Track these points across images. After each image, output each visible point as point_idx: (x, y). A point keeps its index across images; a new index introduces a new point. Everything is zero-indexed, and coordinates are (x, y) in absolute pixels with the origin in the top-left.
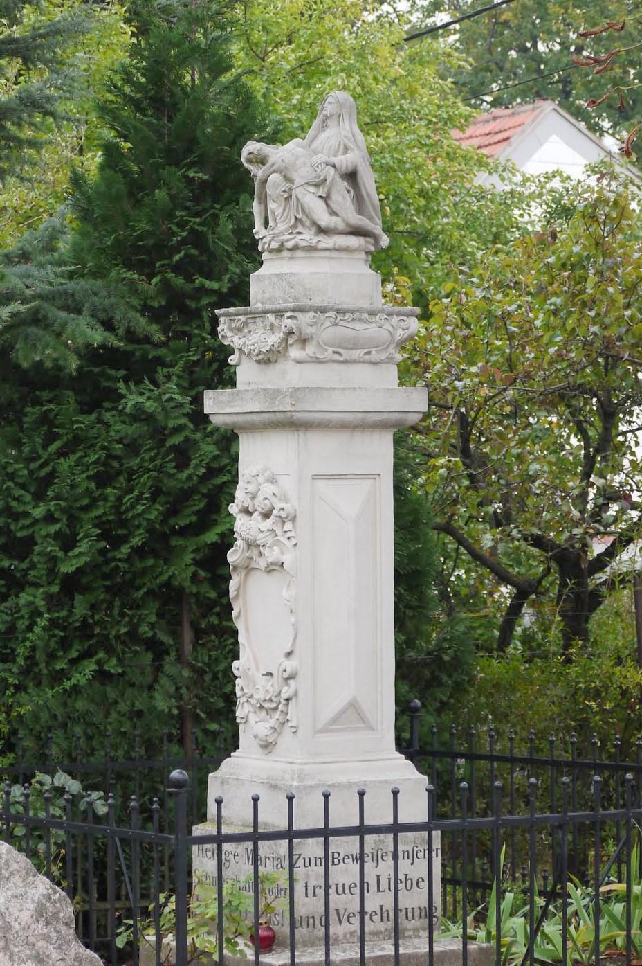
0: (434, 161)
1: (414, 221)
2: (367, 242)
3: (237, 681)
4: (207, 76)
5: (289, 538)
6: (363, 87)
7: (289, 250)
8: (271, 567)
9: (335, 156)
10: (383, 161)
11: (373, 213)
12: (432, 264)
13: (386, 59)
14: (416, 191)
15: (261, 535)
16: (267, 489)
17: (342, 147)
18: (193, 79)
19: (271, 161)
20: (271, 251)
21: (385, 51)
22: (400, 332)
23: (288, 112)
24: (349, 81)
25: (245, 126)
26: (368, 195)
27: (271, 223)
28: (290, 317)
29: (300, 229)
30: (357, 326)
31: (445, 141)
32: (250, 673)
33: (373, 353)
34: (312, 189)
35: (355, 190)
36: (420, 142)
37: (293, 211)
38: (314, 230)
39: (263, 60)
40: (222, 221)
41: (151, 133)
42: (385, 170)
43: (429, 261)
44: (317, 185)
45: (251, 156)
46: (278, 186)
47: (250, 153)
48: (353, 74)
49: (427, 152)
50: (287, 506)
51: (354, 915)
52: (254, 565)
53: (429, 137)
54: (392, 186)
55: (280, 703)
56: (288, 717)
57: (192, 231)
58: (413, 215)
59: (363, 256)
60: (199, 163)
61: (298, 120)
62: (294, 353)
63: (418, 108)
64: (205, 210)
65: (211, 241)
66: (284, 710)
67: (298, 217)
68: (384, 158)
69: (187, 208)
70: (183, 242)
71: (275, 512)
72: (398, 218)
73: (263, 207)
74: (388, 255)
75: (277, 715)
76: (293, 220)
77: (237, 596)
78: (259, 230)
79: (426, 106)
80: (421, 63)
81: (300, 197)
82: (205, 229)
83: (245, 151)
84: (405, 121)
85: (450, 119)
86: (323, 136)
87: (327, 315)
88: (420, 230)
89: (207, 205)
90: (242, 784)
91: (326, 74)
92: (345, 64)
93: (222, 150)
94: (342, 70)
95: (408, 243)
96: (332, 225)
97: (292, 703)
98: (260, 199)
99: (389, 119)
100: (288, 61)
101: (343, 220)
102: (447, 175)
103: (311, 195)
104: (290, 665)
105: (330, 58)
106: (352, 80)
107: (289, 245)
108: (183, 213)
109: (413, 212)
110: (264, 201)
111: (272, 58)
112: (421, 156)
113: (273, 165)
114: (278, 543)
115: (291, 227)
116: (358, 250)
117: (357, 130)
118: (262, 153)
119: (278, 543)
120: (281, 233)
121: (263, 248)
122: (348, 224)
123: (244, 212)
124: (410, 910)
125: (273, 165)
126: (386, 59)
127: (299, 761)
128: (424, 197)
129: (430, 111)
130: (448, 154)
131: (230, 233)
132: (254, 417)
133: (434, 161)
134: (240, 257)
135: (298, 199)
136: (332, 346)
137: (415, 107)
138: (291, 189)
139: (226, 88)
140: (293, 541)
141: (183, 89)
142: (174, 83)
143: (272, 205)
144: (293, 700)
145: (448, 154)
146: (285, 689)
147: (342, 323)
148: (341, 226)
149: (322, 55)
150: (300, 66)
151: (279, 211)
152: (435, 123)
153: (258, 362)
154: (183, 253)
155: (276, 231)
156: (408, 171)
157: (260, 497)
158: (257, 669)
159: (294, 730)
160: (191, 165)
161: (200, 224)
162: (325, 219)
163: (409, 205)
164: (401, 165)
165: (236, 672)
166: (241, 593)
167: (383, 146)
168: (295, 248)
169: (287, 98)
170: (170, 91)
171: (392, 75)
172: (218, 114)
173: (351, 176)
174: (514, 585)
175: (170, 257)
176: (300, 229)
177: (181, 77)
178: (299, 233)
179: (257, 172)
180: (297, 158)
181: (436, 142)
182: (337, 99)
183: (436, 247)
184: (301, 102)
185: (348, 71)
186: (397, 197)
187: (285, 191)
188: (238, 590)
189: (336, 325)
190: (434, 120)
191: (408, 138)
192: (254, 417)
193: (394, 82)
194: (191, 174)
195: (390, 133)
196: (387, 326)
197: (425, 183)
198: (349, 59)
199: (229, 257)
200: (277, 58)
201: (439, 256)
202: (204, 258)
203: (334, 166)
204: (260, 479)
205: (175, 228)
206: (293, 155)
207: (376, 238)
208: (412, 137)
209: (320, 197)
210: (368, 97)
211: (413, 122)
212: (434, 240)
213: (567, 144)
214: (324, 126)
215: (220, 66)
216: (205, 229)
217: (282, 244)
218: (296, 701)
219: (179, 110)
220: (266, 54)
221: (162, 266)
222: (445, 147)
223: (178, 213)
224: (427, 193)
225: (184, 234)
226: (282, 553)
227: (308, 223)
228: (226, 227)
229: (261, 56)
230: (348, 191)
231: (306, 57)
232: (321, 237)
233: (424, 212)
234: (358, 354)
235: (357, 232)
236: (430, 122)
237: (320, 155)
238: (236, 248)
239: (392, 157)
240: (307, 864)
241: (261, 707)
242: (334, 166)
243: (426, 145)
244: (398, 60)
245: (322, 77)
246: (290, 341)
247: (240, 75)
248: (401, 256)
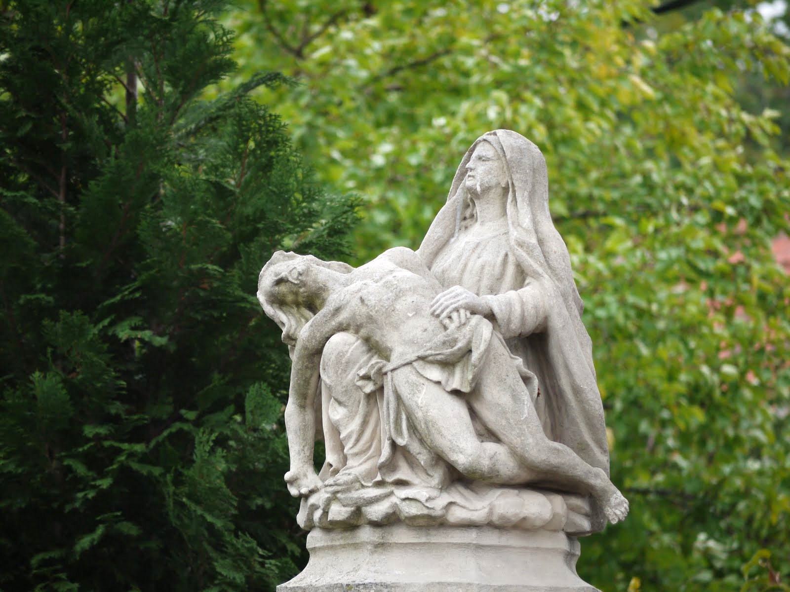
0: (729, 313)
1: (675, 467)
2: (571, 508)
4: (167, 89)
6: (551, 126)
9: (493, 290)
10: (601, 313)
11: (587, 438)
12: (719, 574)
13: (609, 59)
14: (682, 389)
17: (511, 270)
18: (130, 97)
19: (333, 299)
20: (330, 527)
21: (608, 38)
23: (363, 185)
24: (515, 112)
25: (261, 215)
26: (577, 391)
27: (331, 457)
29: (404, 473)
31: (756, 267)
34: (435, 373)
35: (543, 381)
36: (694, 268)
37: (386, 428)
38: (437, 476)
39: (299, 54)
40: (200, 451)
41: (23, 230)
42: (605, 334)
43: (711, 567)
44: (447, 364)
45: (283, 288)
46: (349, 364)
47: (280, 282)
48: (527, 95)
49: (711, 293)
53: (715, 254)
54: (622, 376)
57: (125, 475)
58: (669, 451)
59: (562, 543)
60: (146, 307)
61: (385, 205)
63: (689, 182)
64: (159, 424)
65: (170, 502)
67: (401, 442)
68: (602, 304)
69: (107, 419)
70: (103, 501)
72: (634, 457)
73: (310, 416)
74: (608, 550)
76: (386, 451)
78: (299, 474)
79: (708, 177)
80: (697, 71)
81: (405, 392)
82: (157, 471)
83: (267, 277)
84: (655, 214)
85: (769, 209)
86: (463, 242)
88: (689, 488)
89: (164, 410)
91: (458, 92)
92: (506, 68)
93: (203, 273)
94: (498, 84)
95: (659, 519)
96: (485, 464)
98: (303, 396)
99: (614, 207)
100: (363, 60)
101: (513, 452)
102: (761, 351)
103: (435, 389)
105: (468, 51)
106: (523, 109)
107: (377, 511)
108: (102, 431)
109: (671, 442)
110: (313, 402)
111: (323, 51)
112: (696, 301)
113: (338, 310)
115: (381, 467)
116: (548, 527)
117: (549, 228)
118: (309, 280)
120: (358, 482)
121: (310, 519)
122: (522, 461)
123: (255, 430)
125: (338, 310)
126: (609, 59)
128: (702, 405)
129: (718, 190)
130: (762, 297)
131: (220, 483)
133: (729, 313)
134: (245, 543)
135: (398, 398)
137: (680, 177)
138: (381, 373)
139: (211, 120)
141: (106, 115)
142: (84, 104)
143: (332, 413)
145: (762, 297)
148: (507, 466)
149: (448, 45)
150: (393, 72)
152: (732, 220)
154: (100, 530)
155: (342, 477)
156: (661, 337)
160: (122, 311)
161: (144, 459)
162: (466, 449)
163: (664, 424)
164: (644, 323)
167: (599, 274)
168: (391, 520)
169: (360, 152)
170: (72, 124)
171: (624, 97)
172: (196, 183)
173: (534, 343)
175: (69, 539)
176: (404, 473)
177: (97, 90)
179: (299, 328)
180: (399, 294)
181: (734, 267)
182: (499, 147)
183: (729, 531)
184: (395, 160)
185: (514, 86)
186: (634, 404)
187: (366, 378)
190: (730, 211)
191: (663, 255)
193: (623, 117)
194: (123, 333)
195: (619, 243)
197: (705, 369)
198: (517, 55)
199: (219, 546)
200: (335, 51)
201: (738, 554)
202: (154, 545)
203: (491, 316)
205: (81, 469)
206: (387, 285)
207: (594, 499)
208: (675, 253)
209: (456, 393)
210: (563, 150)
211: (674, 215)
212: (724, 514)
213: (466, 488)
214: (467, 215)
215: (202, 64)
216: (157, 471)
217: (358, 512)
219: (96, 173)
220: (308, 39)
221: (45, 563)
222: (756, 280)
223: (89, 431)
224: (710, 395)
225: (105, 483)
227: (423, 458)
228: (213, 467)
229: (295, 45)
230: (526, 380)
231: (409, 50)
232: (457, 495)
233: (703, 443)
235: (545, 481)
236: (718, 216)
237: (457, 289)
238: (235, 519)
239: (622, 303)
242: (491, 316)
243: (705, 274)
244: (640, 60)
245: (447, 101)
247: (247, 87)
248: (643, 553)
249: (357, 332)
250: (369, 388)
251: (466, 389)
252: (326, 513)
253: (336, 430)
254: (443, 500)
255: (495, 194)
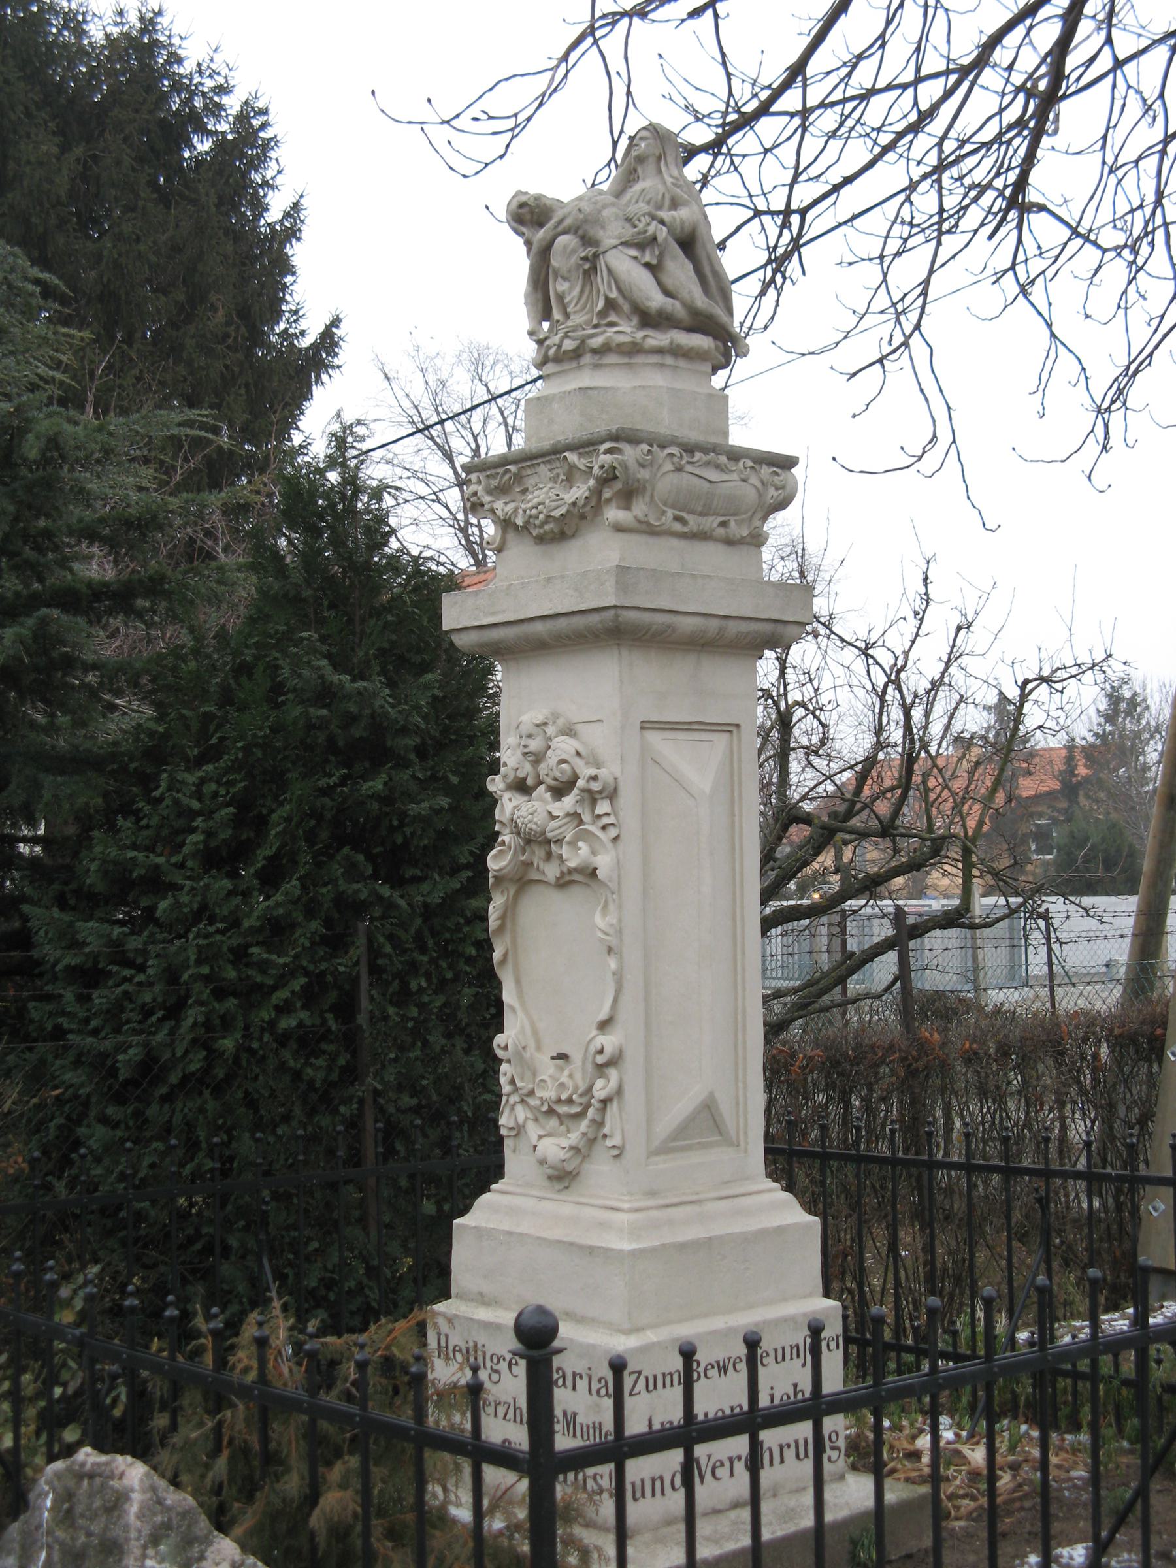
3: (504, 1067)
5: (604, 828)
7: (595, 351)
8: (568, 878)
15: (554, 824)
16: (564, 746)
22: (772, 492)
28: (607, 452)
29: (613, 317)
30: (713, 475)
32: (527, 1055)
33: (732, 524)
34: (634, 252)
38: (635, 320)
44: (641, 246)
50: (602, 772)
51: (722, 1465)
52: (534, 875)
55: (589, 1105)
56: (606, 1130)
62: (613, 514)
66: (598, 1118)
71: (581, 783)
75: (584, 1125)
77: (501, 929)
87: (667, 451)
90: (511, 1245)
97: (613, 1108)
101: (684, 304)
104: (609, 1042)
107: (596, 342)
114: (586, 836)
119: (586, 836)
124: (801, 1443)
125: (561, 221)
127: (626, 1206)
132: (539, 627)
135: (609, 270)
136: (673, 507)
140: (613, 832)
144: (615, 1103)
146: (600, 1083)
147: (689, 468)
151: (572, 296)
153: (540, 540)
157: (552, 758)
158: (539, 1048)
159: (616, 1152)
162: (656, 300)
165: (500, 1053)
166: (509, 925)
174: (234, 994)
178: (612, 324)
188: (503, 918)
189: (679, 469)
192: (539, 627)
196: (754, 480)
204: (550, 730)
209: (647, 265)
218: (620, 1109)
226: (594, 853)
227: (626, 307)
234: (710, 523)
240: (651, 1387)
241: (551, 1112)
246: (607, 494)
249: (576, 232)
250: (587, 266)
251: (654, 262)
252: (560, 346)
253: (560, 298)
254: (640, 335)
255: (652, 160)
